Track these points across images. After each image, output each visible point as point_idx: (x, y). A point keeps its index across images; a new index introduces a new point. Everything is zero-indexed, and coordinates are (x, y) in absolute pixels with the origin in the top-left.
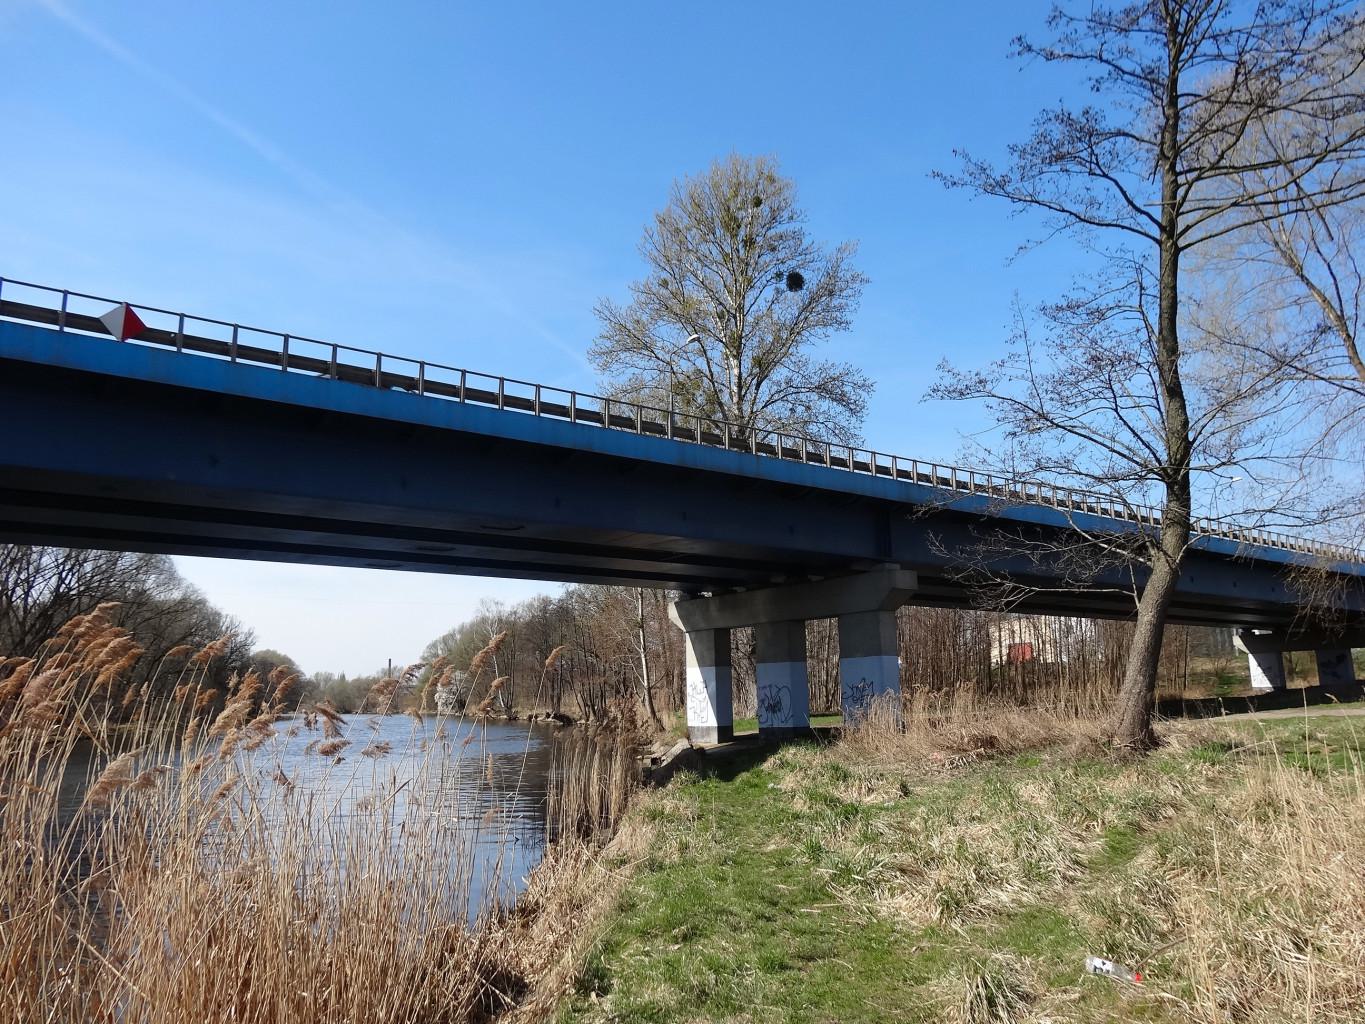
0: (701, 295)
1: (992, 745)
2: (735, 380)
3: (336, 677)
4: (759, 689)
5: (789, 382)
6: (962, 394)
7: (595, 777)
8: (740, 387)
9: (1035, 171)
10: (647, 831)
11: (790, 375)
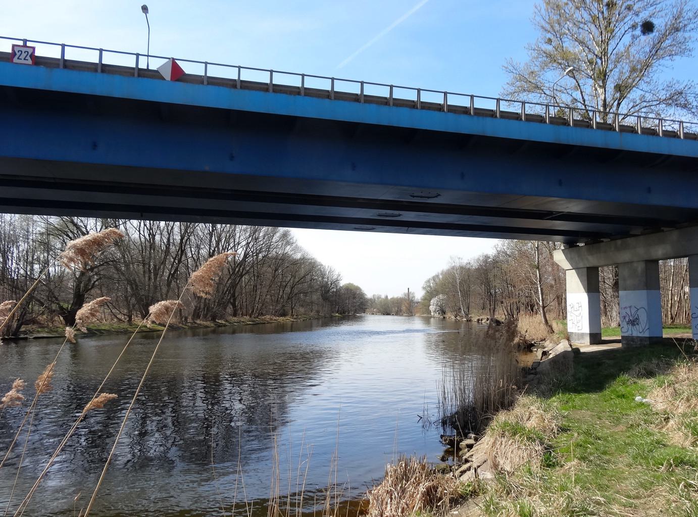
3: (383, 297)
11: (643, 93)
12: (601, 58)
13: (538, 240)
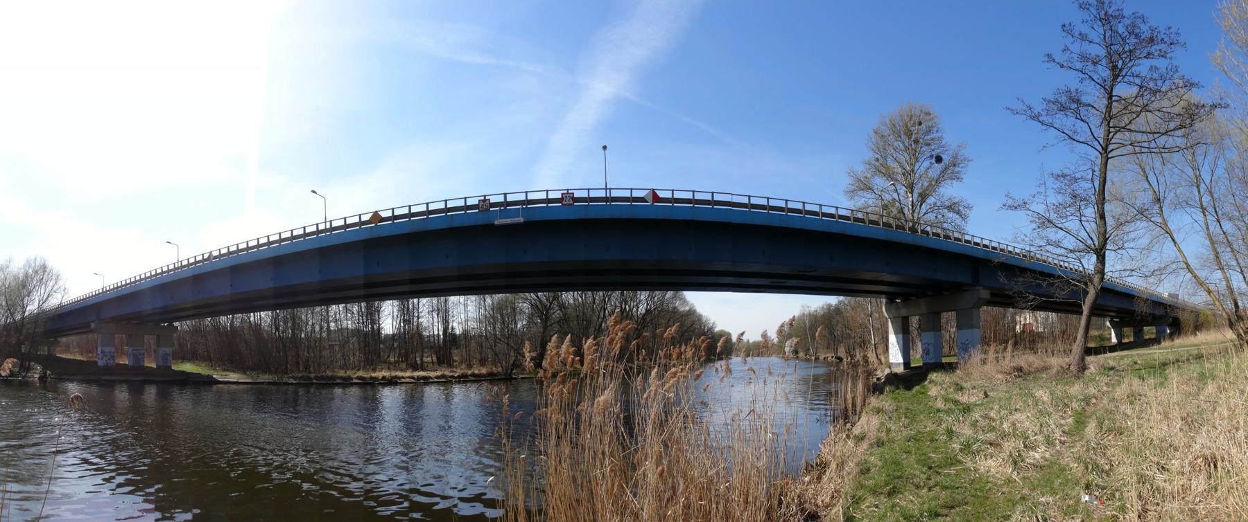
0: (895, 165)
1: (1021, 371)
2: (910, 203)
4: (922, 344)
5: (935, 204)
6: (1016, 208)
7: (849, 390)
8: (913, 206)
9: (1054, 113)
10: (875, 421)
12: (910, 174)
13: (870, 297)
